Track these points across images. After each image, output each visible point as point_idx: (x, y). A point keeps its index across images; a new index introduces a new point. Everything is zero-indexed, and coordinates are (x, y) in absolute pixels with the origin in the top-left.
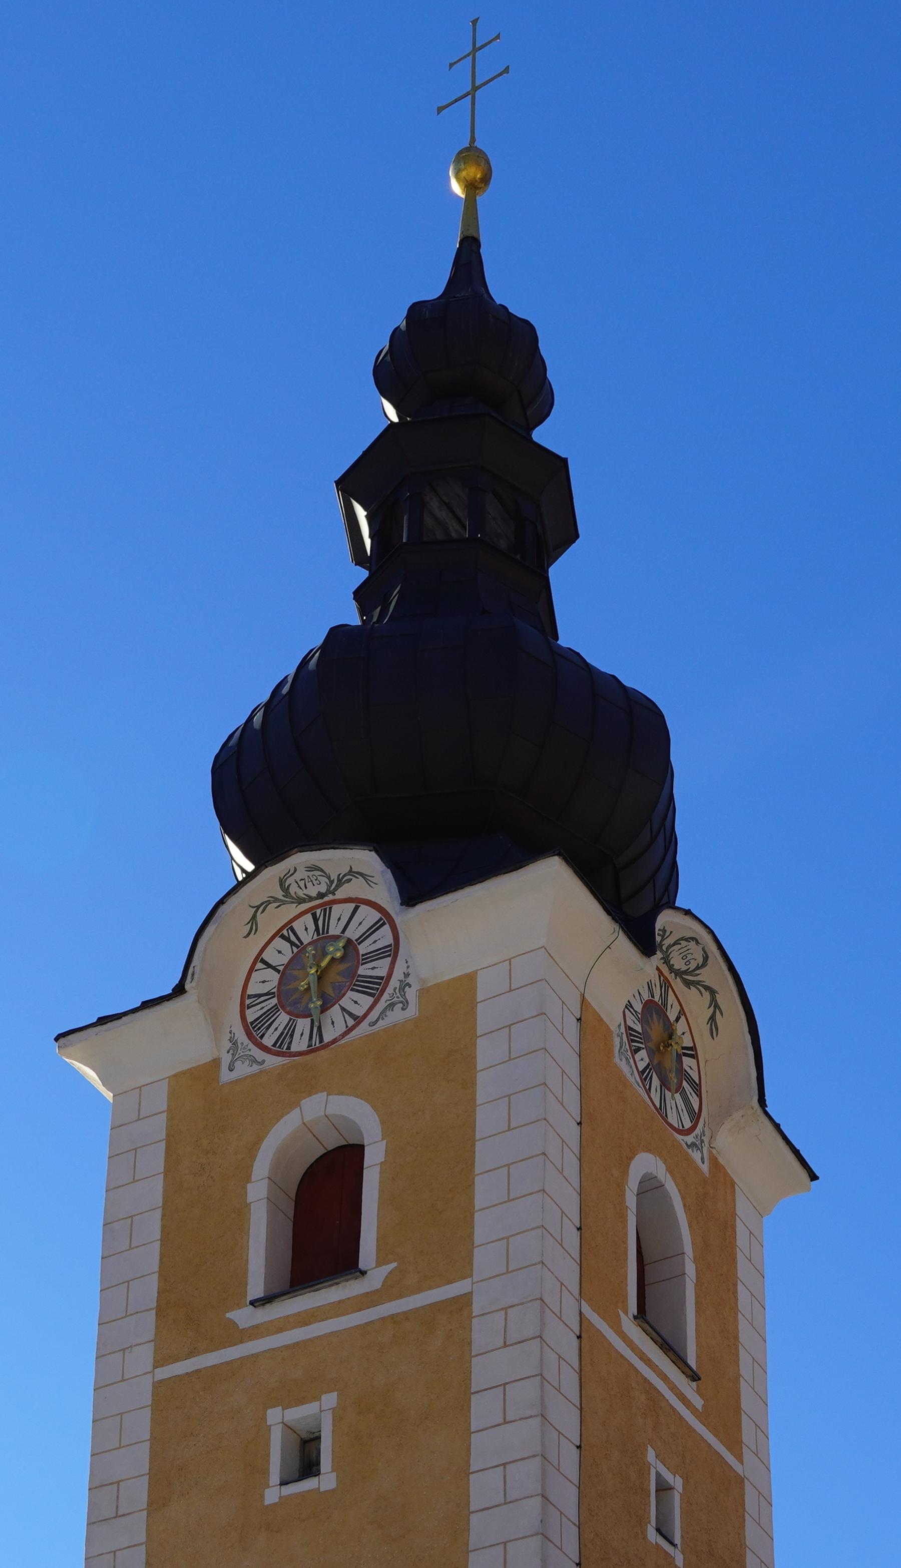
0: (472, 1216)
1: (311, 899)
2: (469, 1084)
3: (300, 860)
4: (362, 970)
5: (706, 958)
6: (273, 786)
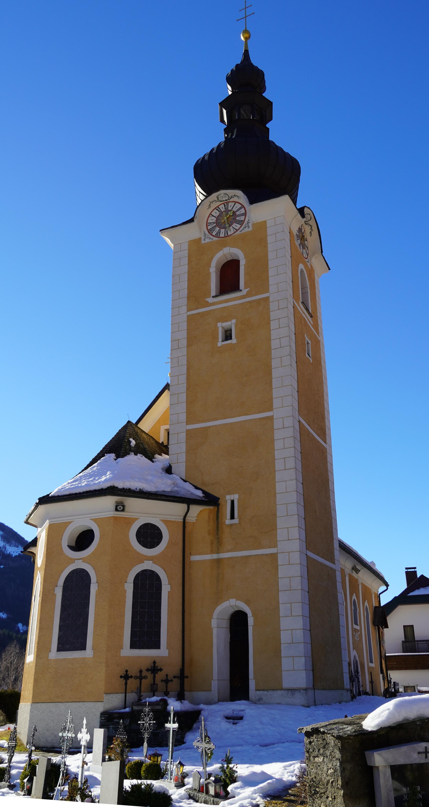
0: (268, 278)
1: (224, 201)
2: (266, 247)
3: (222, 192)
4: (237, 218)
5: (311, 218)
6: (211, 173)
